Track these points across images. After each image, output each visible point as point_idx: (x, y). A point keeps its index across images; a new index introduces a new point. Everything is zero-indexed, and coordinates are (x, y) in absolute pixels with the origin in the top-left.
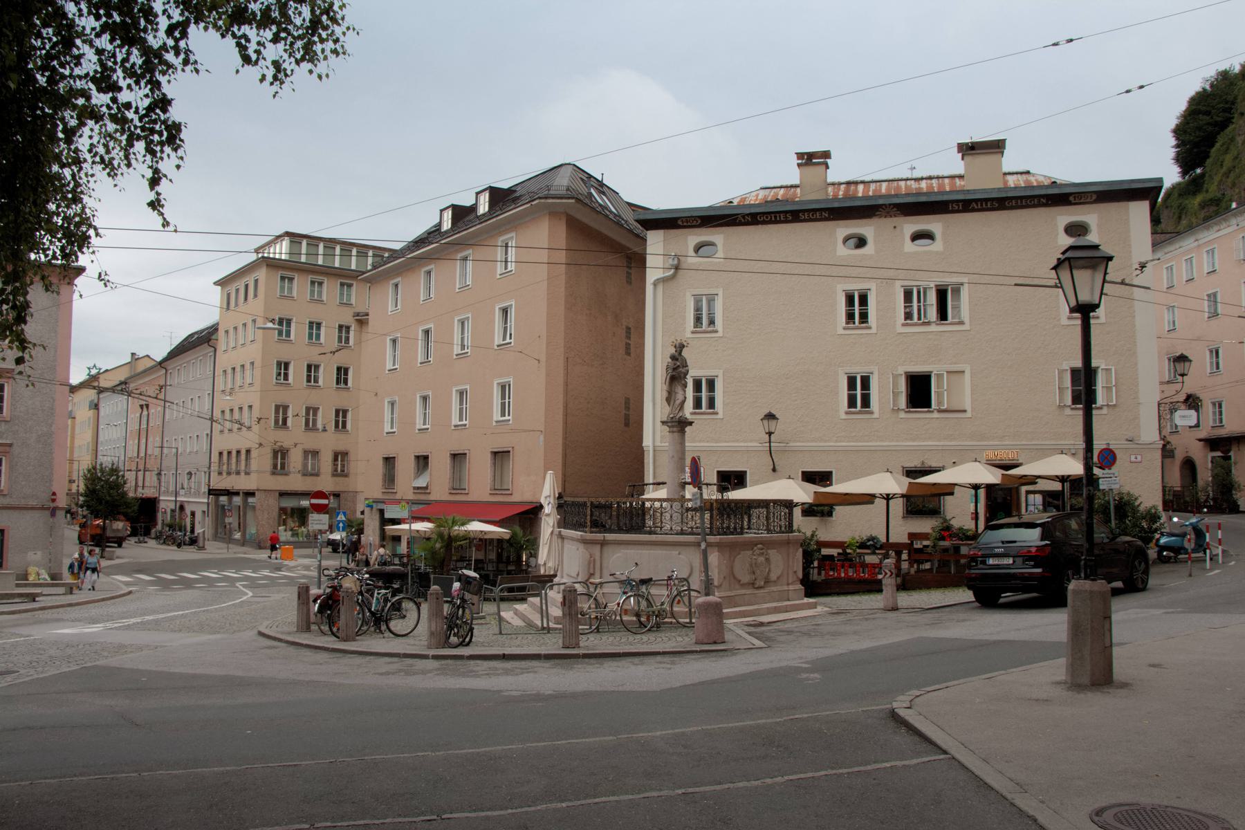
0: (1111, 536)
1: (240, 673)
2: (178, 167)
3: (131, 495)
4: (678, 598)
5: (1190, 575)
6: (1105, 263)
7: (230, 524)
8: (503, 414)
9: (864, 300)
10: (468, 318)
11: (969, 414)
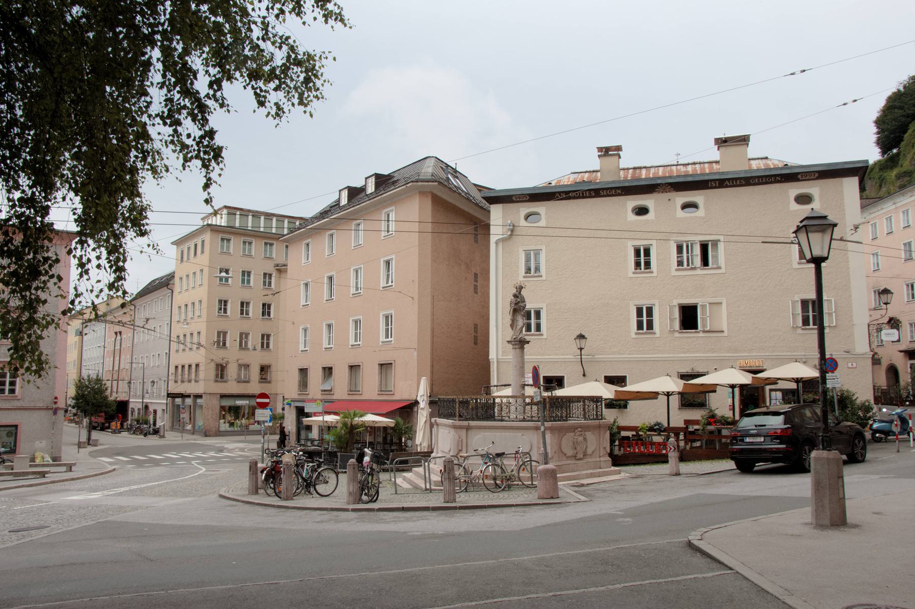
0: (836, 422)
1: (214, 524)
2: (220, 175)
3: (111, 398)
4: (523, 466)
5: (898, 451)
6: (831, 228)
7: (184, 418)
8: (387, 337)
9: (647, 252)
10: (361, 268)
11: (726, 334)
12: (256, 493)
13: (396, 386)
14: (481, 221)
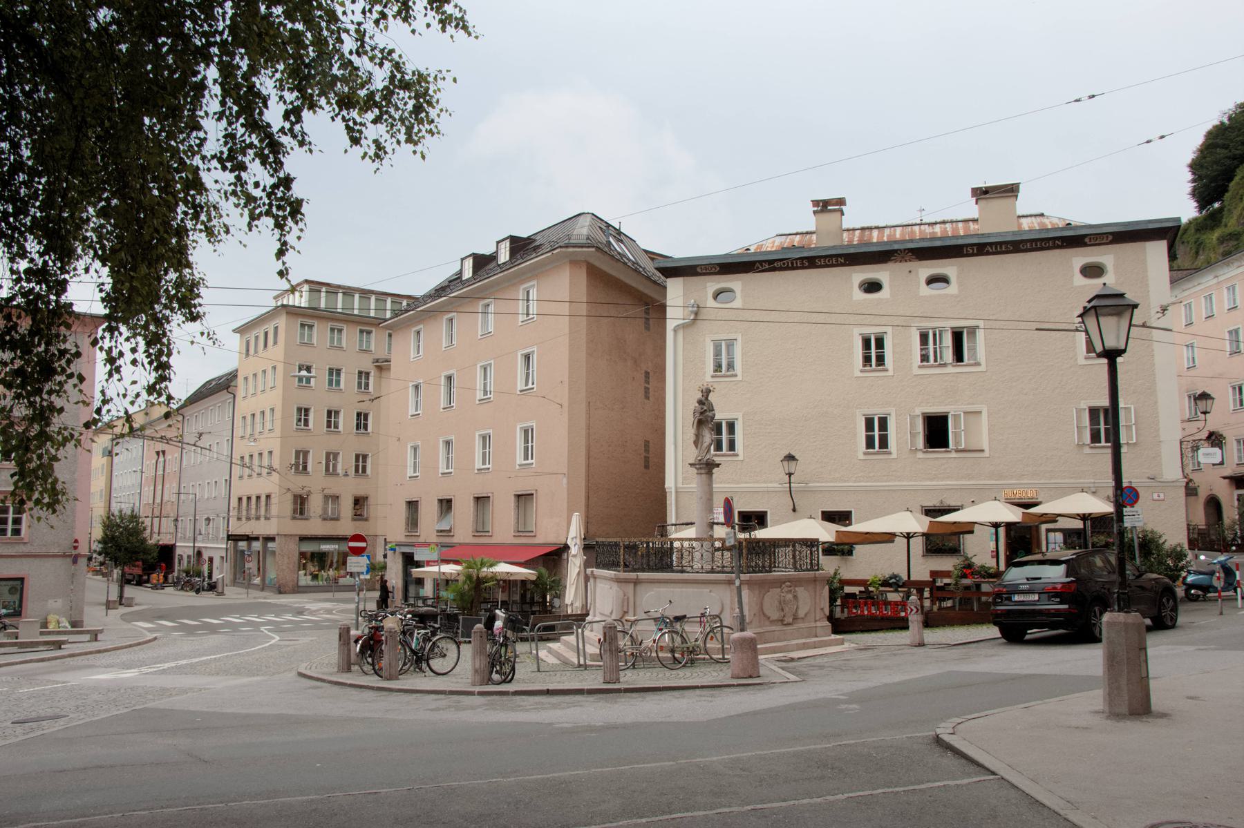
0: (1137, 573)
1: (291, 712)
2: (299, 238)
3: (152, 542)
4: (711, 634)
5: (1221, 614)
6: (1130, 310)
7: (250, 569)
8: (526, 458)
9: (880, 343)
10: (490, 364)
11: (986, 454)
12: (349, 670)
13: (538, 524)
14: (654, 300)
